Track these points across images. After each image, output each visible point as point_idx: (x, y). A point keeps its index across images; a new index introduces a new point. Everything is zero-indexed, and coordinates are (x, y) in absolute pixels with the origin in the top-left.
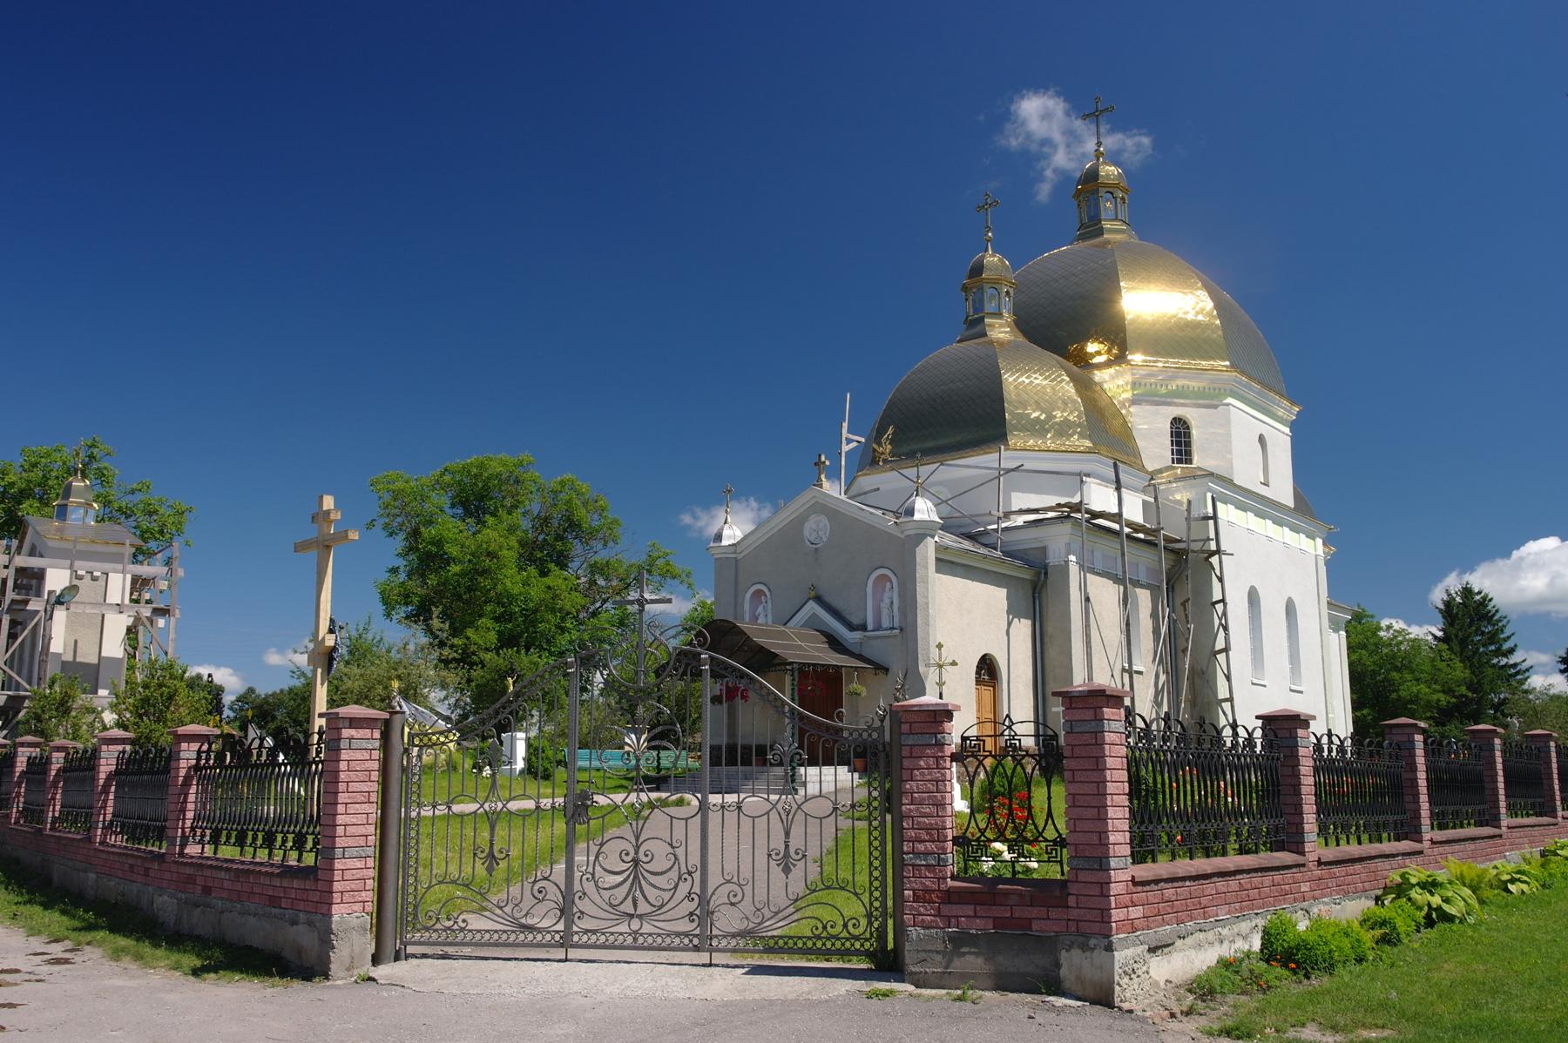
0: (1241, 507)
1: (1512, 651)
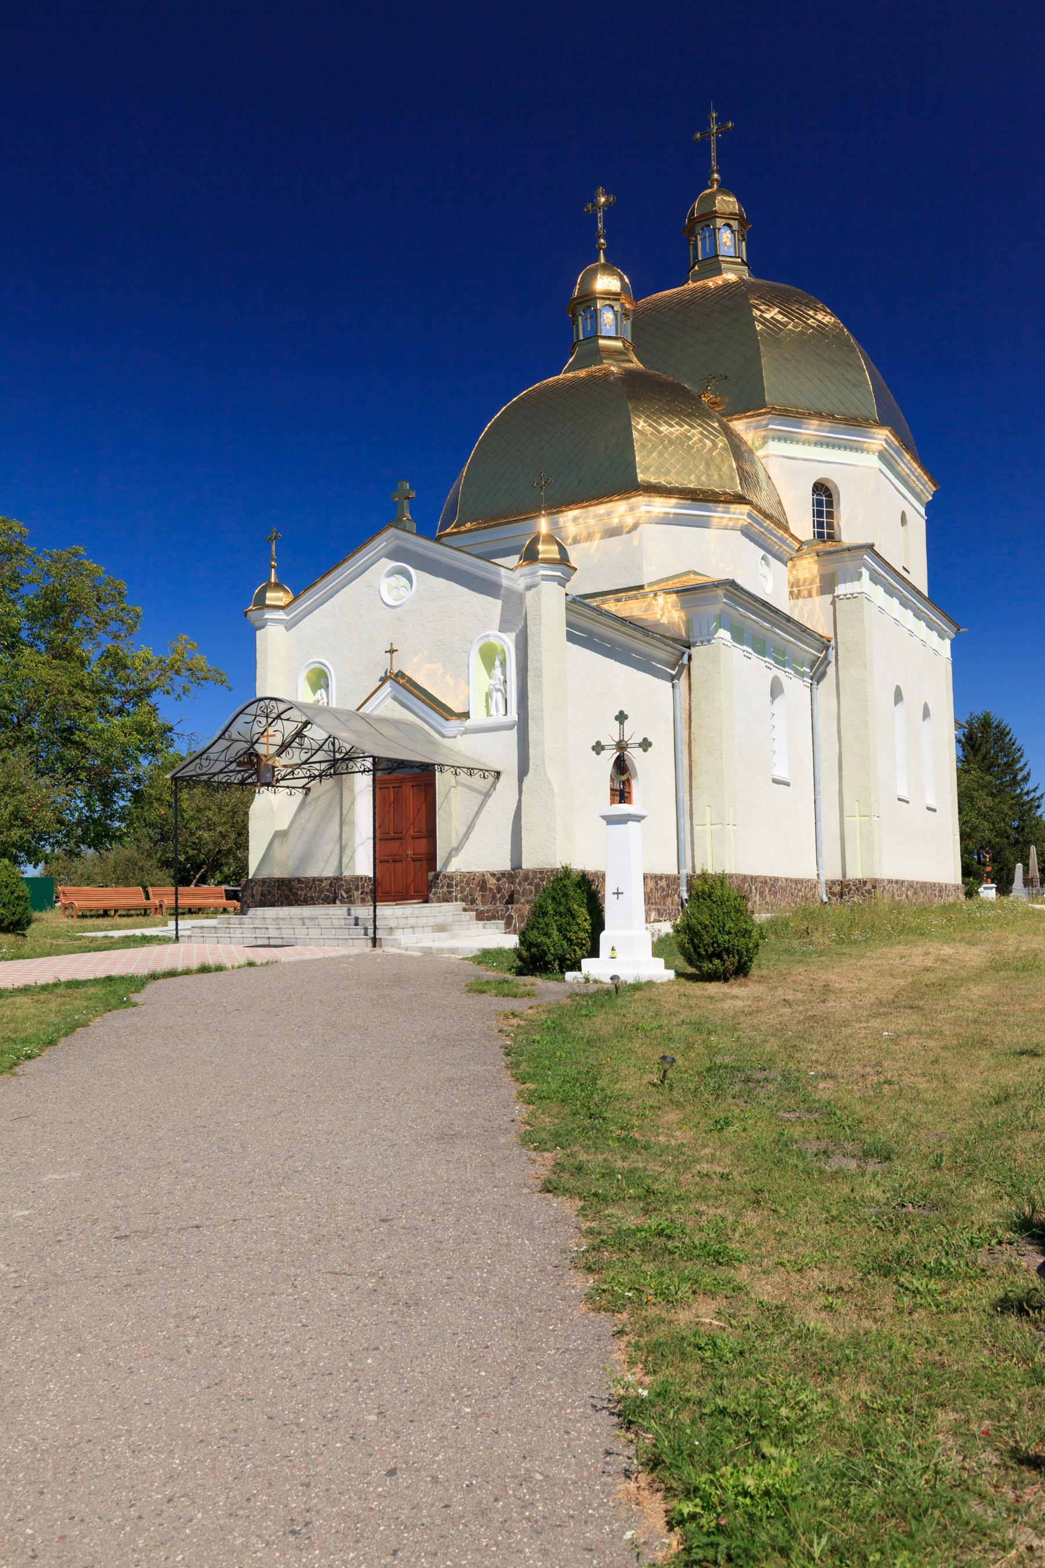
0: (890, 592)
1: (1025, 779)
